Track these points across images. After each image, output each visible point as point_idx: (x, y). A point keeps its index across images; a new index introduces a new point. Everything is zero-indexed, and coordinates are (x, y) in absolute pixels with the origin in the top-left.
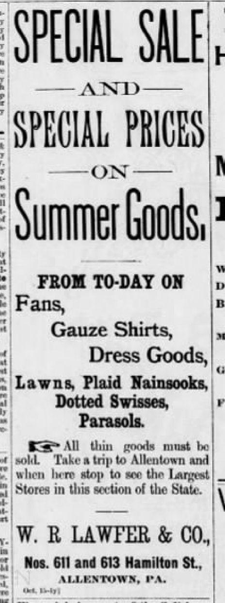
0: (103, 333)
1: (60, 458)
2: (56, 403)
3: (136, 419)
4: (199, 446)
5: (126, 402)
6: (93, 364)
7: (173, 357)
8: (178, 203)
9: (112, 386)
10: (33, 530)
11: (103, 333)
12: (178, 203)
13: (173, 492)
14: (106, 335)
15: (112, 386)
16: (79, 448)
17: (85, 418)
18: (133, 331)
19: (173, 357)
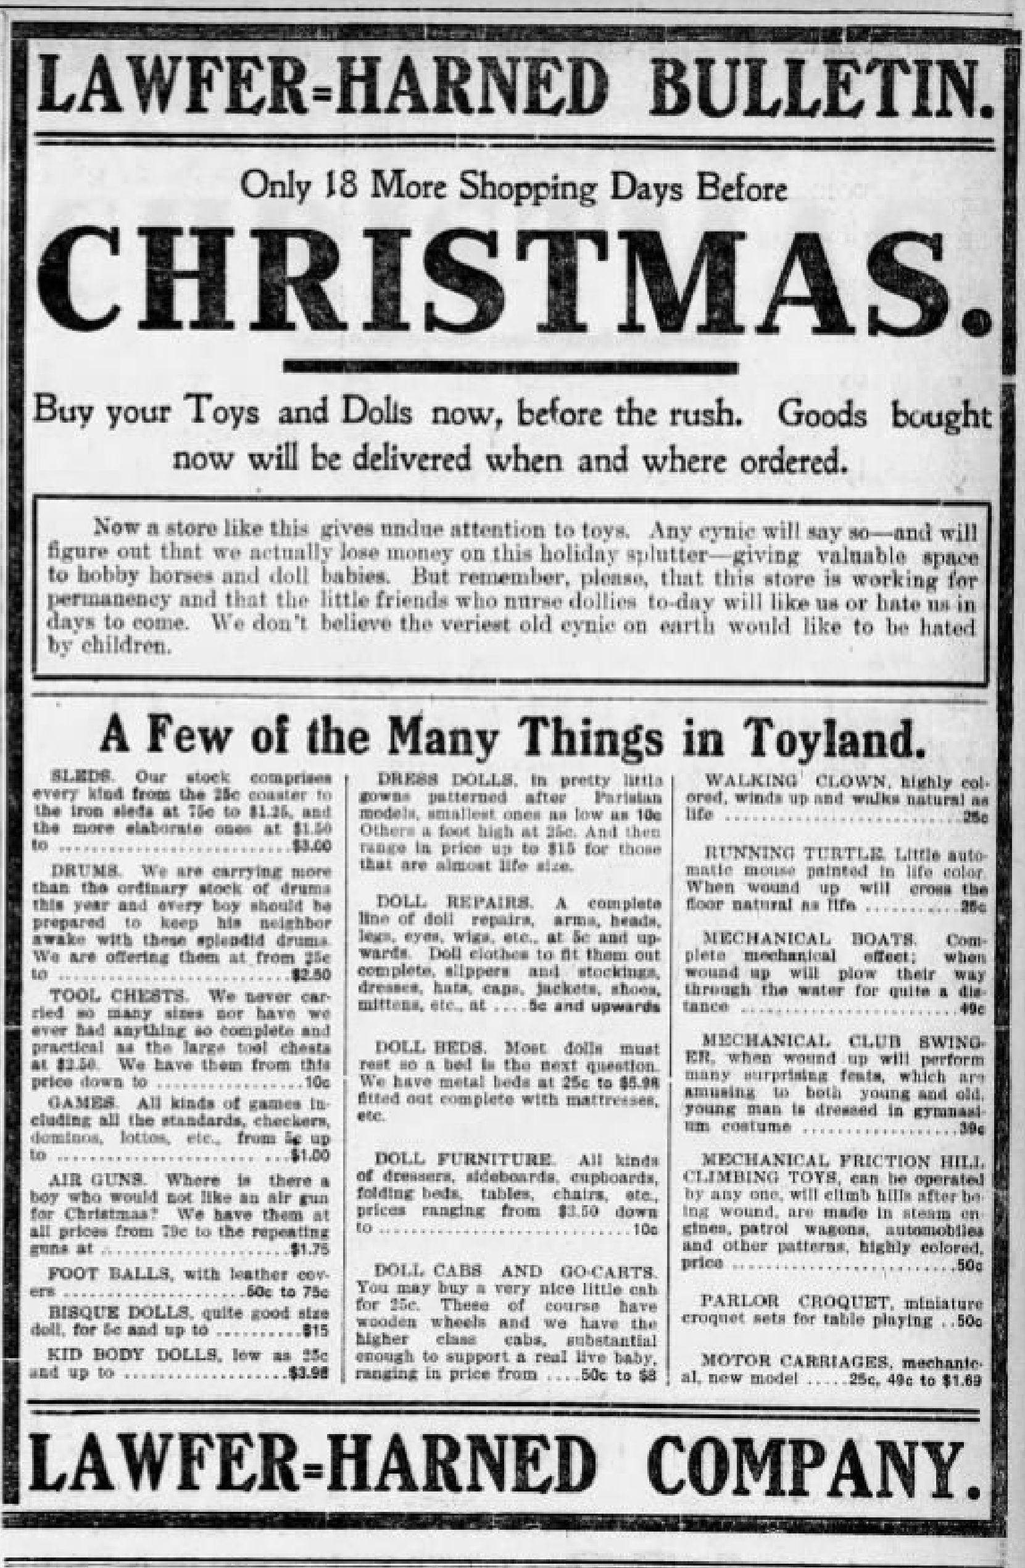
0: (359, 745)
1: (765, 727)
2: (651, 104)
3: (403, 410)
4: (152, 574)
5: (481, 416)
6: (348, 426)
7: (820, 419)
8: (807, 1472)
9: (888, 750)
10: (499, 738)
11: (359, 745)
12: (807, 1472)
13: (315, 467)
14: (366, 749)
15: (888, 750)
16: (309, 578)
17: (808, 1455)
18: (565, 740)
19: (820, 419)
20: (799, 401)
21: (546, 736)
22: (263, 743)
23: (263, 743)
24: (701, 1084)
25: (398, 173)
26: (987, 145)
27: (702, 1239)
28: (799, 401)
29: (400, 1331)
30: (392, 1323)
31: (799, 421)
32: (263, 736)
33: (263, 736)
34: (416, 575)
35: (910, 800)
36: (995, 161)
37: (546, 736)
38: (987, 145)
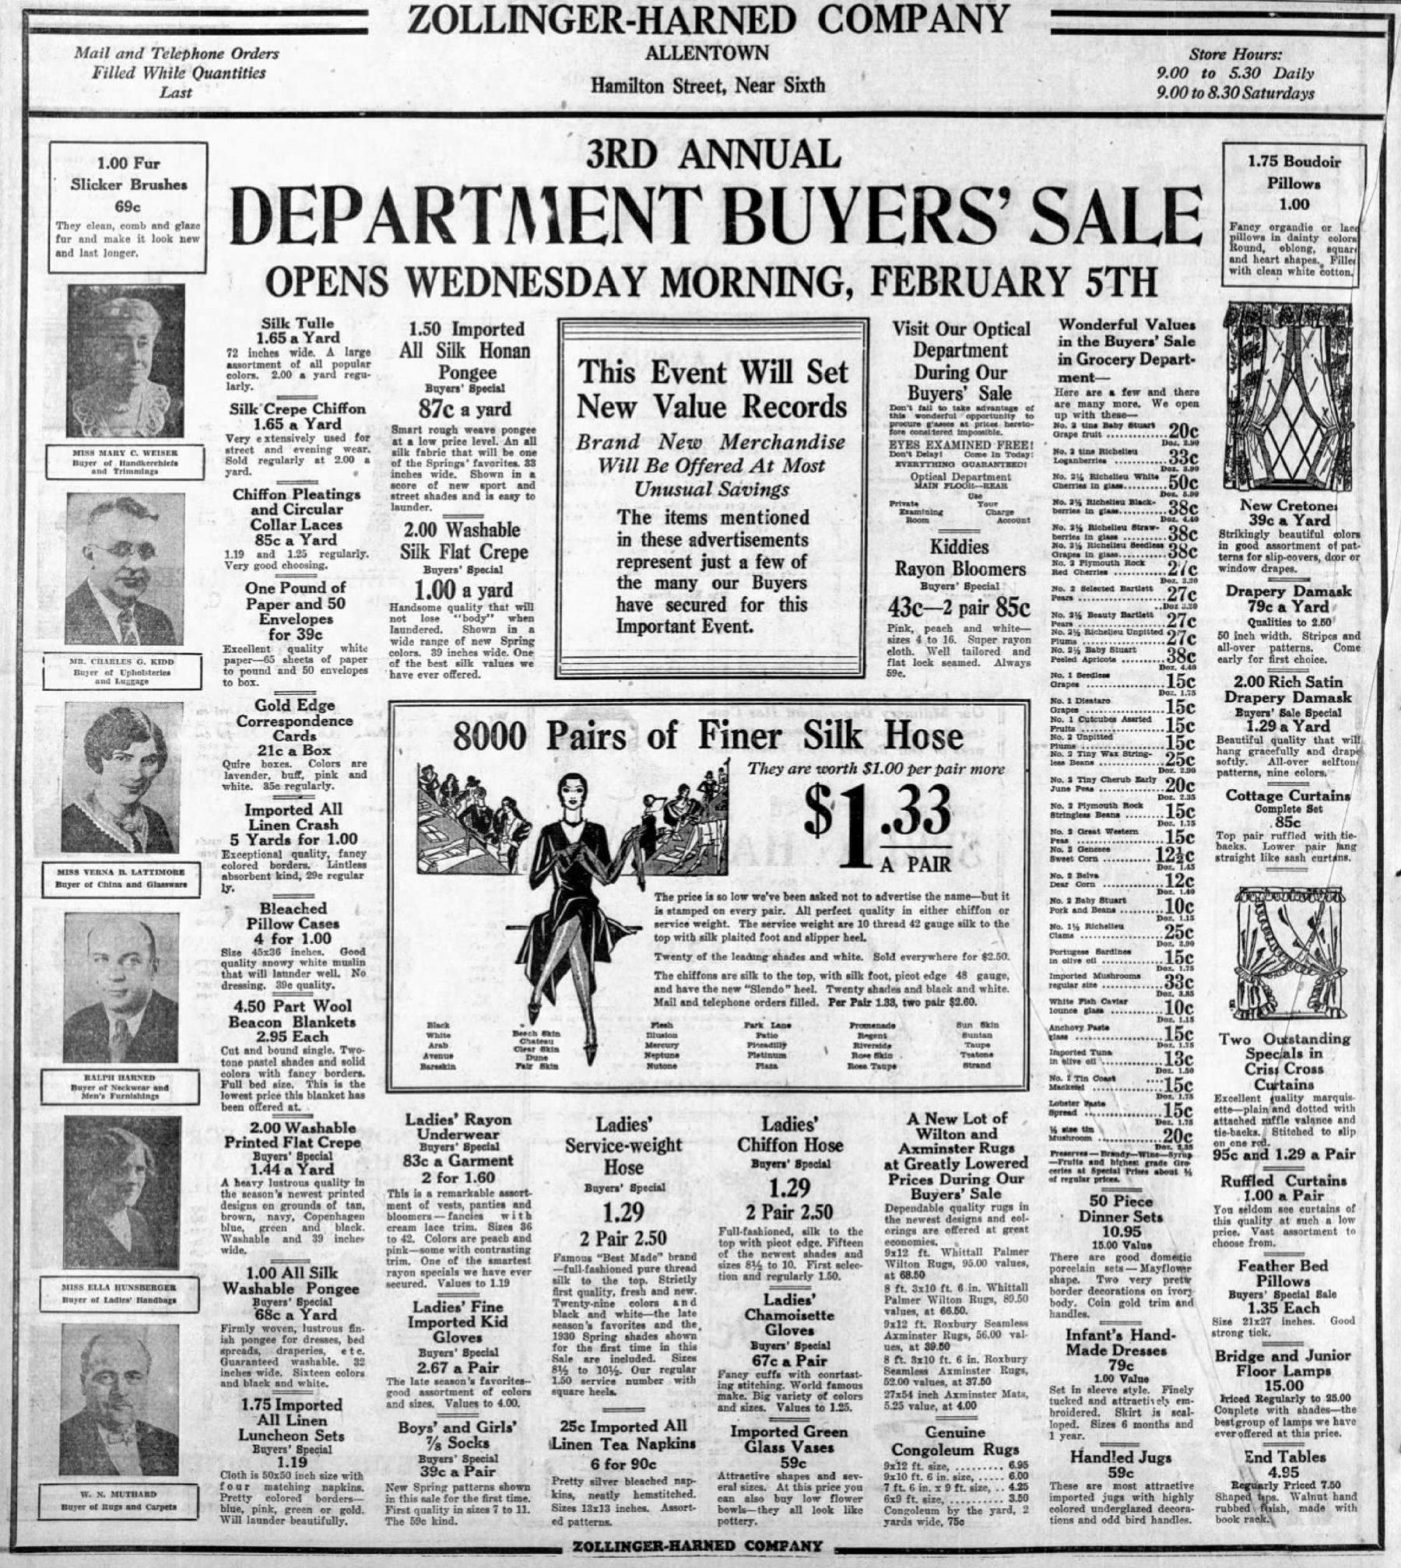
11: (957, 743)
20: (838, 270)
21: (596, 371)
22: (657, 742)
23: (657, 742)
24: (1226, 853)
25: (905, 723)
26: (446, 1062)
27: (276, 445)
28: (838, 270)
29: (412, 481)
30: (408, 475)
31: (570, 29)
32: (657, 736)
33: (657, 736)
34: (891, 733)
35: (1115, 806)
36: (1385, 41)
37: (596, 371)
38: (446, 1062)
